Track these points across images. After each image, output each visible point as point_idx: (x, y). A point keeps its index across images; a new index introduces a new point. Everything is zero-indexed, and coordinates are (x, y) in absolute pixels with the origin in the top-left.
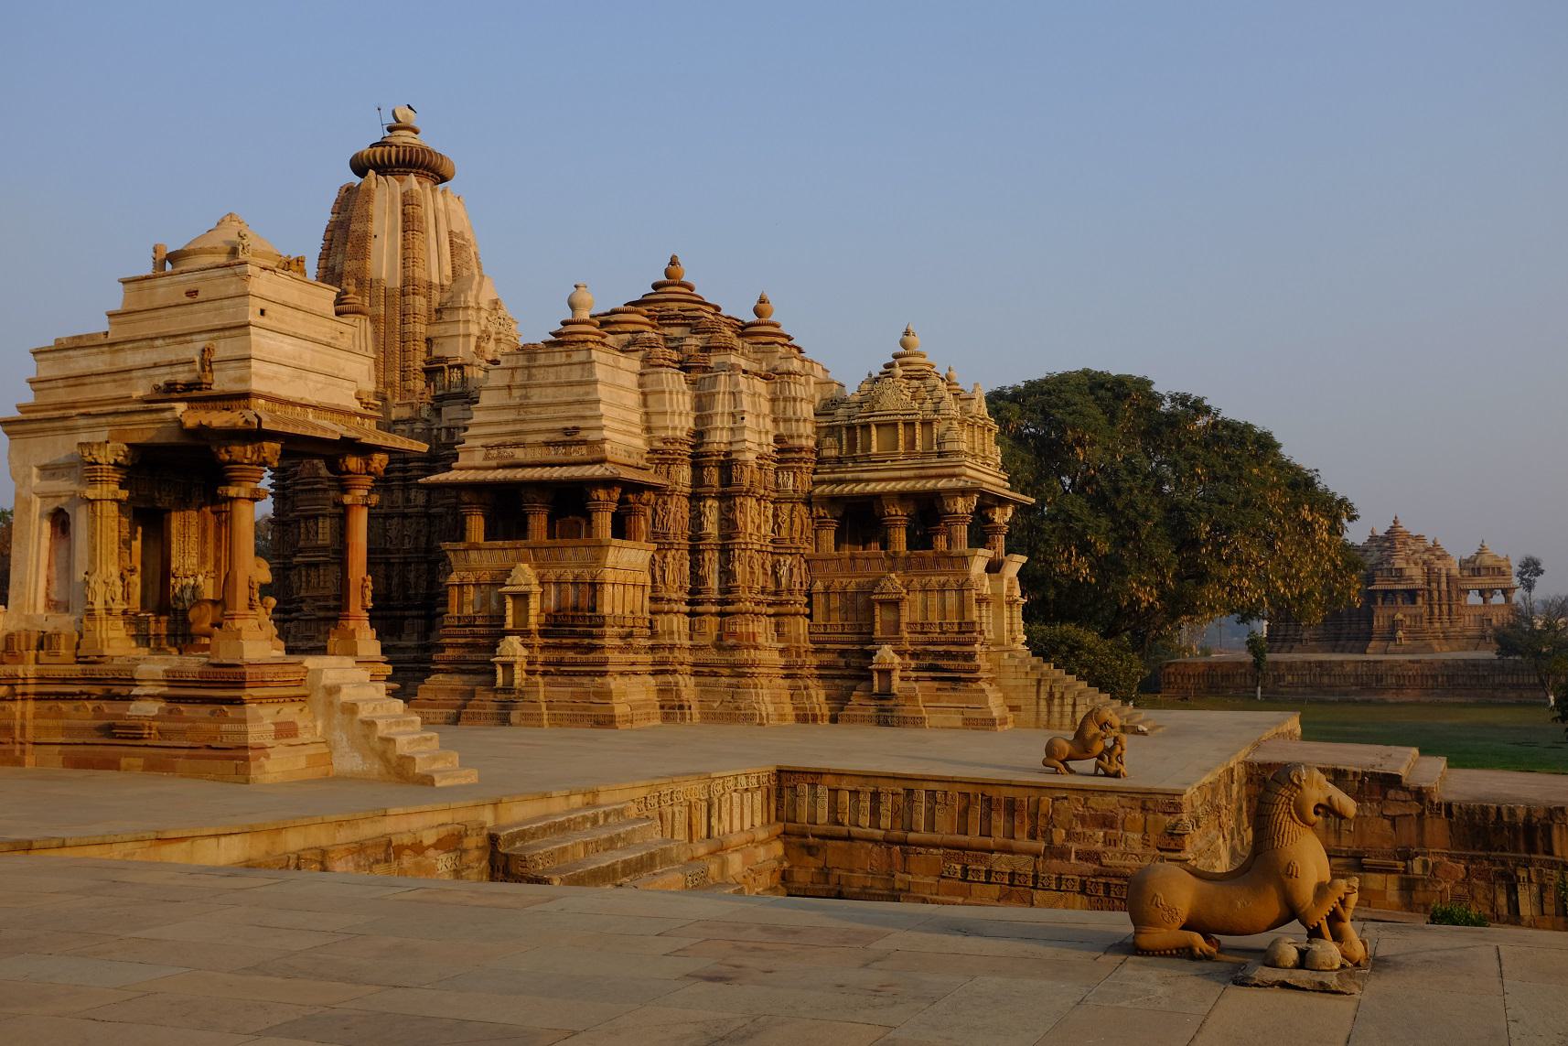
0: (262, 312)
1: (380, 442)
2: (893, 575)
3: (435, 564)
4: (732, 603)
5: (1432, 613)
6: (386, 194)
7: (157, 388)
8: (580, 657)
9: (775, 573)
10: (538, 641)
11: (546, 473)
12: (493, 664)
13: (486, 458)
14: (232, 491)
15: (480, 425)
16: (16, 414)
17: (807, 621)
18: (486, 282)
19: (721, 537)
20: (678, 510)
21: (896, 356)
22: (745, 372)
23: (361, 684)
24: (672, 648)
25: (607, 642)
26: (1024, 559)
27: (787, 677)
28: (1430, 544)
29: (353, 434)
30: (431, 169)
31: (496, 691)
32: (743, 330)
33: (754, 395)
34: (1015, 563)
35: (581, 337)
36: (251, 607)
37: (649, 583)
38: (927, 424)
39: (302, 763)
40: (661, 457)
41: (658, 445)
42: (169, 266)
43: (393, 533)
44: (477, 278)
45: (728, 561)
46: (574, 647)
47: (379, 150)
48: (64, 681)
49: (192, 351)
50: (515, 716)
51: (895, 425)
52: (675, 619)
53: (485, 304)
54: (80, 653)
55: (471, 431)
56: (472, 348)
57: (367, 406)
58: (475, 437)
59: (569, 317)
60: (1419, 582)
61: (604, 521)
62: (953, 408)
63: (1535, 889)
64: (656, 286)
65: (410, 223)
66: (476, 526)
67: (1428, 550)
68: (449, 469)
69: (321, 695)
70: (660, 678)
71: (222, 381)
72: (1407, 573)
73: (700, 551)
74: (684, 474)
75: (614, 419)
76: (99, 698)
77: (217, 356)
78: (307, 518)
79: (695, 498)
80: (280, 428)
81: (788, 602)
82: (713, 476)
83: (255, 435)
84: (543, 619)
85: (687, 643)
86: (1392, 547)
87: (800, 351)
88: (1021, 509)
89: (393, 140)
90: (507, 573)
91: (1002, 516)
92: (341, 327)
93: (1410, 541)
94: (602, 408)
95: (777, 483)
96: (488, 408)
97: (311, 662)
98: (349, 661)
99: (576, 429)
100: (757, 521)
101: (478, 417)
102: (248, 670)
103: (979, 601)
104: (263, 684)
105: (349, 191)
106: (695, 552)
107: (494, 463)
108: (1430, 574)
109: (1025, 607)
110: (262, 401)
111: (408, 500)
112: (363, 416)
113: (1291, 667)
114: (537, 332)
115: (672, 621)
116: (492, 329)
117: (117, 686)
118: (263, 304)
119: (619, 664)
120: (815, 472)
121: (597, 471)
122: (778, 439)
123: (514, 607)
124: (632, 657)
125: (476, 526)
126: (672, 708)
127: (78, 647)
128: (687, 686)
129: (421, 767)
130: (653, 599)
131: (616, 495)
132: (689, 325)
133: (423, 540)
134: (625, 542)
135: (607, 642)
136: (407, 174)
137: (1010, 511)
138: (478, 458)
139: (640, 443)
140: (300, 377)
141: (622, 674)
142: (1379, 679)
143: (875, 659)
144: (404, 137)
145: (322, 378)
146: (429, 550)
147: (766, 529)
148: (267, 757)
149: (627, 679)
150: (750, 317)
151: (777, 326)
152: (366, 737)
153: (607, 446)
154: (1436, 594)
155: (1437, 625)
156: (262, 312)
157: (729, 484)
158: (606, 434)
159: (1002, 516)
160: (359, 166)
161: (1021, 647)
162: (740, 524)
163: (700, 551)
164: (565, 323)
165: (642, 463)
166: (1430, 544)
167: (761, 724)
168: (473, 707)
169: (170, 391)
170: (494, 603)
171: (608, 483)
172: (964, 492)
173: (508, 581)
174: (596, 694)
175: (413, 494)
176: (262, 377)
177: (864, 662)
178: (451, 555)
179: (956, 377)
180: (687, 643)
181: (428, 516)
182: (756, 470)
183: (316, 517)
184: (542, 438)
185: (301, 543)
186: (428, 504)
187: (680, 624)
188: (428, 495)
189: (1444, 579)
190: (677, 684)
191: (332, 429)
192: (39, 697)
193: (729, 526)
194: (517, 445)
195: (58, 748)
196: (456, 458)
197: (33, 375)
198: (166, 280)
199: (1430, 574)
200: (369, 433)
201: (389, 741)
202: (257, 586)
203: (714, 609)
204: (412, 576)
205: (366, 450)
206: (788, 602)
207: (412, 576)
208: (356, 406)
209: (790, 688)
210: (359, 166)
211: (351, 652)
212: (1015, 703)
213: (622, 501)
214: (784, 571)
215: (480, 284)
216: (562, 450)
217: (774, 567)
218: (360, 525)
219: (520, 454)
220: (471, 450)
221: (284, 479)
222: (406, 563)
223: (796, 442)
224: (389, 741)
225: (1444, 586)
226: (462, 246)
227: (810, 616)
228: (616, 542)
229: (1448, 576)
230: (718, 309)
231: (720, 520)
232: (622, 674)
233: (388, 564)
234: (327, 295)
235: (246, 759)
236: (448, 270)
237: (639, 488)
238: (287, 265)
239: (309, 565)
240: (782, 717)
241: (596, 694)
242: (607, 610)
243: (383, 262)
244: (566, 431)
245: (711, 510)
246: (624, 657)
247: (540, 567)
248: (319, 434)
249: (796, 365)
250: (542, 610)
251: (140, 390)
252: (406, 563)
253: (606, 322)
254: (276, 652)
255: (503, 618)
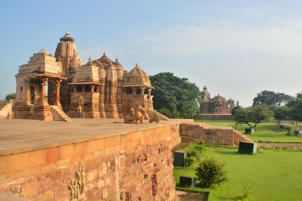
0: (47, 61)
1: (61, 78)
2: (133, 98)
3: (69, 96)
4: (111, 101)
5: (223, 108)
6: (64, 44)
7: (33, 71)
8: (89, 109)
9: (117, 97)
10: (83, 106)
11: (85, 83)
12: (77, 110)
13: (77, 81)
14: (42, 84)
15: (76, 76)
16: (17, 75)
17: (121, 104)
18: (78, 56)
19: (109, 92)
20: (103, 88)
21: (135, 67)
22: (113, 69)
23: (58, 109)
24: (102, 108)
25: (93, 106)
26: (153, 96)
27: (118, 112)
28: (223, 98)
29: (57, 77)
30: (71, 40)
31: (78, 113)
32: (114, 63)
33: (114, 72)
34: (152, 97)
35: (90, 64)
36: (44, 99)
37: (99, 99)
38: (138, 77)
39: (51, 119)
40: (101, 81)
41: (101, 79)
42: (35, 56)
43: (64, 92)
44: (77, 56)
45: (110, 96)
46: (88, 107)
47: (64, 38)
48: (22, 108)
49: (38, 66)
50: (80, 117)
51: (134, 77)
52: (103, 104)
53: (78, 59)
54: (24, 105)
55: (75, 77)
56: (76, 66)
57: (59, 73)
58: (75, 78)
59: (89, 61)
60: (221, 104)
61: (93, 90)
62: (143, 75)
63: (215, 140)
64: (102, 57)
65: (67, 48)
66: (75, 90)
67: (223, 99)
68: (72, 82)
69: (53, 110)
70: (100, 112)
71: (41, 70)
72: (220, 102)
73: (106, 94)
74: (104, 83)
75: (94, 76)
76: (26, 110)
77: (41, 67)
78: (52, 90)
79: (105, 87)
80: (48, 76)
81: (119, 102)
82: (108, 84)
83: (45, 77)
84: (84, 103)
85: (104, 107)
86: (218, 98)
87: (122, 66)
88: (152, 89)
89: (66, 36)
90: (79, 97)
91: (150, 90)
92: (56, 63)
93: (221, 97)
94: (93, 76)
95: (117, 85)
96: (77, 74)
97: (52, 106)
98: (57, 106)
99: (89, 77)
100: (114, 90)
101: (76, 75)
102: (44, 107)
103: (145, 102)
104: (46, 108)
105: (59, 43)
106: (105, 94)
107: (78, 82)
108: (223, 102)
109: (153, 103)
110: (46, 73)
111: (66, 87)
112: (59, 75)
113: (202, 116)
114: (85, 63)
115: (102, 104)
116: (79, 63)
117: (28, 109)
118: (47, 60)
119: (94, 110)
120: (123, 83)
121: (92, 83)
122: (118, 79)
123: (82, 103)
124: (96, 109)
125: (75, 90)
126: (102, 116)
127: (24, 104)
128: (104, 113)
129: (65, 119)
130: (99, 101)
131: (94, 86)
132: (106, 62)
133: (68, 93)
134: (96, 93)
135: (93, 106)
136: (68, 41)
137: (151, 90)
138: (76, 81)
139: (98, 79)
140: (51, 70)
141: (95, 111)
142: (215, 118)
143: (131, 110)
144: (68, 36)
145: (54, 70)
146: (69, 94)
147: (116, 91)
148: (47, 117)
149: (95, 112)
150: (115, 61)
151: (119, 63)
152: (59, 115)
153: (93, 79)
154: (224, 105)
155: (224, 110)
156: (47, 61)
157: (110, 85)
158: (93, 78)
159: (150, 90)
160: (61, 40)
161: (152, 109)
162: (112, 90)
163: (106, 94)
164: (88, 62)
165: (98, 82)
166: (223, 98)
167: (114, 118)
168: (74, 115)
169: (36, 71)
170: (78, 101)
171: (93, 85)
172: (144, 87)
173: (79, 98)
174: (91, 114)
175: (67, 86)
176: (47, 70)
177: (129, 110)
178: (72, 94)
179: (143, 70)
180: (104, 107)
181: (69, 89)
182: (114, 83)
183: (54, 90)
184: (84, 78)
185: (52, 93)
186: (69, 88)
187: (103, 104)
188: (69, 87)
189: (225, 103)
190: (103, 113)
191: (55, 76)
192: (19, 110)
193: (110, 91)
194: (80, 79)
195: (21, 117)
196: (73, 81)
197: (19, 70)
198: (35, 57)
199: (223, 102)
200: (59, 77)
201: (62, 116)
202: (45, 97)
203: (108, 102)
204: (67, 98)
205: (59, 79)
206: (119, 102)
207: (67, 98)
208: (58, 73)
209: (118, 114)
210: (61, 40)
211: (57, 105)
212: (150, 116)
213: (95, 87)
214: (118, 97)
215: (77, 57)
216: (87, 80)
217: (117, 97)
218: (58, 88)
219: (81, 81)
220: (75, 80)
221: (49, 84)
222: (66, 96)
223: (120, 79)
224: (62, 116)
225: (225, 104)
226: (75, 51)
227: (122, 104)
228: (94, 93)
229: (226, 103)
230: (111, 60)
231: (109, 90)
232: (95, 111)
233: (64, 96)
234: (55, 59)
235: (44, 118)
236: (73, 55)
237: (98, 85)
238: (50, 55)
239: (53, 96)
240: (117, 117)
241: (91, 114)
242: (93, 102)
243: (64, 54)
244: (88, 77)
245: (108, 89)
246: (95, 109)
247: (84, 96)
248: (53, 77)
249: (121, 68)
250: (84, 102)
251: (32, 71)
252: (66, 96)
253: (94, 62)
254: (48, 105)
255: (78, 103)
